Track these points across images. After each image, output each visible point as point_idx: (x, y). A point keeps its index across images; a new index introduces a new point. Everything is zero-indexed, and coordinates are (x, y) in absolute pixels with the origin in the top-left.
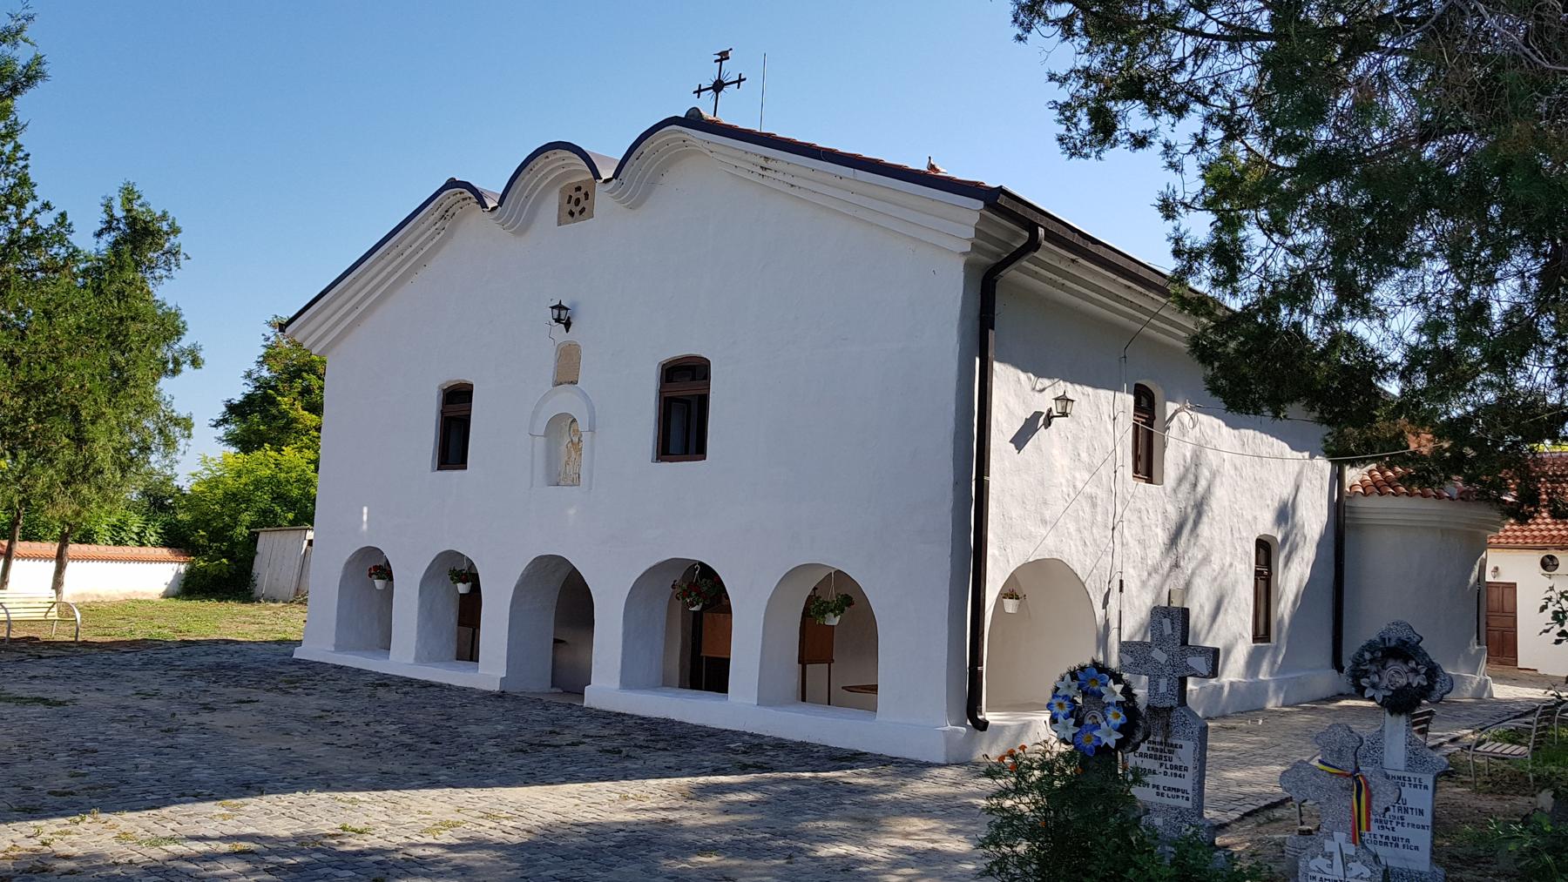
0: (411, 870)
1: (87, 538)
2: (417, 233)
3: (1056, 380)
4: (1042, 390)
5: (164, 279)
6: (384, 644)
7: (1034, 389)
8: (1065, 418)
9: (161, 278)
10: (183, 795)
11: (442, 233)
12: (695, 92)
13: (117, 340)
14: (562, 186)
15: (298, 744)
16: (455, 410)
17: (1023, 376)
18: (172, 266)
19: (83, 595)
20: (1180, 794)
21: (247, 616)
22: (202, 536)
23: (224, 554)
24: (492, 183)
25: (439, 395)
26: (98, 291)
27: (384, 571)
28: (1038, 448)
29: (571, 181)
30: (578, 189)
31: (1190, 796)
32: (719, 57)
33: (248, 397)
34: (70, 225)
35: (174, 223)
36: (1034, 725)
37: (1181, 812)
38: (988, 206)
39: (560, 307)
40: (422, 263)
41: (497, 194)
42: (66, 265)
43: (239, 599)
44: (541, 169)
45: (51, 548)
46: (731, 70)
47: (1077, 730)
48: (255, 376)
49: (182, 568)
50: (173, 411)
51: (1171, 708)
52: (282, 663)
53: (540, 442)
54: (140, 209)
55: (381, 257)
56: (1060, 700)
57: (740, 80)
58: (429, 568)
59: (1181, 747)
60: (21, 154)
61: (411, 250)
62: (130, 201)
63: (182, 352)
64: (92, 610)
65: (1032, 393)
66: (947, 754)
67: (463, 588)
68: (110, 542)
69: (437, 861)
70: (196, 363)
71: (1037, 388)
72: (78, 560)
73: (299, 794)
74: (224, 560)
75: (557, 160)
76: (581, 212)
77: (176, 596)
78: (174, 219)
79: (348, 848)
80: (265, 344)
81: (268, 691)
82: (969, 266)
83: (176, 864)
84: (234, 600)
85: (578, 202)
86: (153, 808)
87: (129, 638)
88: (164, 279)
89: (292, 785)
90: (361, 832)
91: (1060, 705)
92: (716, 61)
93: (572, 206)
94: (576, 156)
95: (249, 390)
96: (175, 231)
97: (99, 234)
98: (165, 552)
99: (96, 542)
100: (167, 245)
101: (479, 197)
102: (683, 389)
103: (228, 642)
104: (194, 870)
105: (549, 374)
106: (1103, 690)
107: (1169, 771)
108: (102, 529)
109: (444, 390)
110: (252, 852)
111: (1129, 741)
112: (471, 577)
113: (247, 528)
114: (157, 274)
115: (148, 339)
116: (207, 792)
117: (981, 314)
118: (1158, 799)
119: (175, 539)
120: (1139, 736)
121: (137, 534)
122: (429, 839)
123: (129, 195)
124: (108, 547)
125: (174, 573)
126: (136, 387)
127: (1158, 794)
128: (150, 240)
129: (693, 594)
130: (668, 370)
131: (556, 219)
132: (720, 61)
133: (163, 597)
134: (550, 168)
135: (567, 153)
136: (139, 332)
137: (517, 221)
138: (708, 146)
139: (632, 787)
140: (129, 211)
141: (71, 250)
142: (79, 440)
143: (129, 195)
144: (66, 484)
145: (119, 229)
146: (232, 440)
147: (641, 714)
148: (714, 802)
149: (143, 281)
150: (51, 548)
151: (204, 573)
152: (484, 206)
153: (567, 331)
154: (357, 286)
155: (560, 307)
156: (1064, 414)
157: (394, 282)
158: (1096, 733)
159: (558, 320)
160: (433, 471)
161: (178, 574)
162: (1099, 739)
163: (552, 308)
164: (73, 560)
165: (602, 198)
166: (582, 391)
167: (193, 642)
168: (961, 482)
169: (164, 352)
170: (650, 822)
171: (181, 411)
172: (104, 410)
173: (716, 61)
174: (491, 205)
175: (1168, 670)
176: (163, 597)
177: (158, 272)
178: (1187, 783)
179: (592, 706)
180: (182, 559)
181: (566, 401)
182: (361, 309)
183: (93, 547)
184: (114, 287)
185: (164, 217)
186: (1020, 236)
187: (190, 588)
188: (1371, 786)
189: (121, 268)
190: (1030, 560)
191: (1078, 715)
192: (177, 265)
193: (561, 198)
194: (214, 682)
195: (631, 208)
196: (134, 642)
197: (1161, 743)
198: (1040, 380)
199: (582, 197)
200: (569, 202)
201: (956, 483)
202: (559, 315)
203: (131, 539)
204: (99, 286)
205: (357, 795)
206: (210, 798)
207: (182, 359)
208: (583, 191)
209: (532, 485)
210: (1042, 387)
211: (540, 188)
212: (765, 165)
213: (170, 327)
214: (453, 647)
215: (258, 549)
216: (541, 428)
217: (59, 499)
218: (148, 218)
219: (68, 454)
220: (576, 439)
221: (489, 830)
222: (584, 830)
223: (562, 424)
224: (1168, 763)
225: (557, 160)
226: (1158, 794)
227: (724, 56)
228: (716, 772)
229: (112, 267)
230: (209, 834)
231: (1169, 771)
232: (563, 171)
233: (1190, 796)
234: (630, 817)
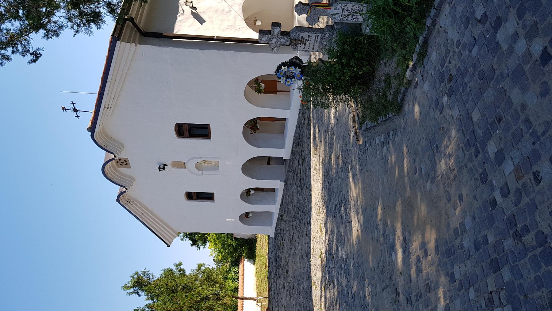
0: (331, 247)
1: (236, 290)
3: (179, 4)
4: (183, 11)
5: (153, 275)
6: (270, 214)
7: (183, 14)
8: (193, 2)
9: (153, 276)
10: (310, 295)
11: (135, 202)
12: (72, 102)
13: (174, 290)
14: (117, 167)
15: (298, 253)
16: (186, 131)
17: (179, 19)
18: (149, 273)
19: (254, 289)
20: (317, 37)
21: (261, 243)
22: (236, 254)
23: (241, 247)
24: (117, 189)
25: (190, 201)
26: (159, 296)
27: (247, 214)
28: (204, 12)
29: (115, 165)
30: (118, 162)
31: (317, 34)
32: (64, 110)
33: (189, 239)
34: (138, 308)
35: (134, 274)
36: (299, 19)
37: (322, 37)
38: (118, 39)
39: (159, 168)
40: (145, 207)
41: (120, 188)
42: (151, 308)
43: (256, 243)
44: (111, 174)
45: (239, 301)
47: (296, 78)
48: (183, 238)
49: (246, 260)
50: (196, 269)
51: (290, 39)
52: (275, 242)
53: (204, 172)
54: (130, 284)
55: (144, 220)
56: (287, 82)
57: (78, 117)
59: (302, 36)
61: (141, 211)
62: (128, 287)
63: (177, 269)
64: (259, 288)
65: (185, 15)
66: (307, 56)
67: (252, 192)
68: (238, 282)
69: (329, 238)
70: (180, 264)
71: (182, 12)
72: (243, 292)
73: (311, 263)
74: (243, 248)
75: (108, 170)
76: (126, 161)
77: (255, 261)
78: (133, 274)
79: (325, 260)
81: (283, 251)
82: (140, 43)
83: (326, 308)
84: (256, 244)
86: (313, 304)
87: (267, 282)
88: (153, 275)
89: (309, 261)
90: (321, 253)
91: (288, 82)
92: (66, 111)
93: (124, 164)
94: (106, 166)
95: (187, 239)
96: (137, 273)
97: (139, 295)
98: (241, 265)
99: (238, 286)
100: (142, 275)
101: (121, 193)
102: (186, 131)
103: (268, 254)
104: (328, 304)
105: (182, 170)
106: (284, 71)
107: (310, 40)
108: (233, 285)
109: (188, 199)
110: (325, 286)
111: (299, 64)
112: (249, 191)
113: (233, 241)
114: (152, 277)
115: (173, 280)
116: (309, 288)
118: (318, 43)
119: (236, 262)
120: (298, 61)
121: (235, 274)
122: (324, 235)
123: (126, 287)
124: (239, 283)
125: (247, 262)
126: (189, 283)
127: (316, 43)
128: (140, 281)
129: (254, 128)
130: (180, 136)
132: (66, 110)
133: (255, 265)
134: (111, 172)
135: (106, 168)
136: (171, 283)
137: (130, 181)
138: (101, 125)
139: (313, 165)
140: (131, 287)
141: (146, 307)
142: (206, 298)
143: (126, 287)
144: (220, 300)
145: (137, 290)
146: (204, 243)
147: (292, 143)
148: (318, 142)
149: (154, 281)
150: (239, 301)
151: (247, 254)
152: (125, 192)
155: (159, 168)
156: (192, 2)
157: (153, 215)
158: (297, 74)
159: (164, 169)
160: (214, 202)
162: (298, 73)
163: (160, 170)
164: (243, 295)
165: (122, 155)
166: (188, 161)
167: (268, 264)
168: (217, 48)
169: (178, 274)
170: (322, 167)
171: (196, 267)
172: (197, 292)
173: (66, 111)
174: (124, 189)
175: (279, 39)
176: (255, 265)
177: (151, 277)
178: (313, 35)
179: (289, 157)
180: (243, 260)
181: (191, 166)
182: (162, 224)
183: (239, 287)
184: (157, 291)
185: (132, 277)
186: (128, 24)
187: (252, 257)
188: (314, 2)
189: (150, 289)
190: (243, 17)
191: (291, 77)
193: (121, 167)
194: (280, 265)
195: (123, 147)
196: (268, 281)
197: (301, 42)
198: (179, 11)
200: (123, 165)
201: (217, 49)
202: (162, 168)
203: (237, 276)
204: (157, 296)
205: (312, 247)
206: (311, 287)
207: (180, 269)
208: (118, 161)
209: (219, 174)
210: (182, 10)
211: (115, 172)
212: (107, 108)
213: (169, 273)
214: (270, 193)
215: (240, 237)
216: (200, 172)
217: (224, 302)
218: (133, 281)
219: (211, 302)
220: (204, 162)
221: (323, 216)
222: (323, 190)
223: (198, 166)
224: (307, 40)
225: (108, 170)
226: (316, 43)
227: (64, 108)
228: (310, 134)
229: (150, 292)
230: (320, 294)
231: (310, 40)
232: (111, 168)
233: (317, 34)
234: (321, 172)
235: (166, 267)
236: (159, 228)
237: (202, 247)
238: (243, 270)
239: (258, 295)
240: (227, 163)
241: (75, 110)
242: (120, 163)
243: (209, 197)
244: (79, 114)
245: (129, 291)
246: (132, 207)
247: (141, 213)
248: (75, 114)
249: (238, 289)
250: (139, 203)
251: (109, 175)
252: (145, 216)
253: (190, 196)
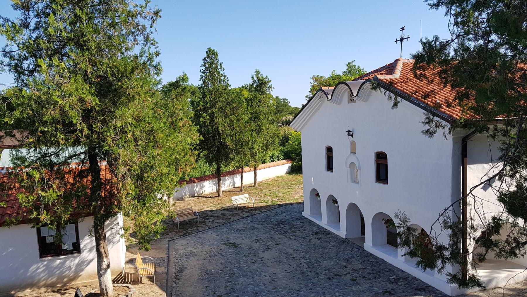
2: (315, 102)
27: (318, 195)
39: (349, 131)
40: (318, 109)
46: (405, 34)
49: (290, 165)
53: (349, 169)
57: (408, 38)
58: (328, 198)
60: (226, 78)
61: (314, 106)
80: (311, 85)
92: (401, 30)
96: (269, 81)
98: (285, 161)
117: (462, 152)
121: (277, 157)
123: (257, 73)
131: (347, 102)
133: (286, 174)
143: (257, 73)
151: (295, 166)
152: (328, 98)
154: (303, 115)
155: (349, 131)
159: (349, 135)
161: (289, 166)
163: (347, 131)
173: (401, 30)
176: (286, 174)
181: (353, 159)
183: (266, 164)
192: (272, 90)
193: (348, 95)
209: (348, 182)
211: (342, 93)
223: (352, 165)
227: (403, 29)
235: (277, 96)
236: (307, 113)
237: (312, 81)
238: (280, 164)
239: (259, 183)
240: (357, 192)
241: (402, 40)
243: (330, 167)
244: (399, 42)
245: (255, 76)
246: (316, 100)
247: (313, 106)
248: (399, 39)
249: (264, 163)
250: (321, 104)
252: (310, 109)
253: (329, 150)
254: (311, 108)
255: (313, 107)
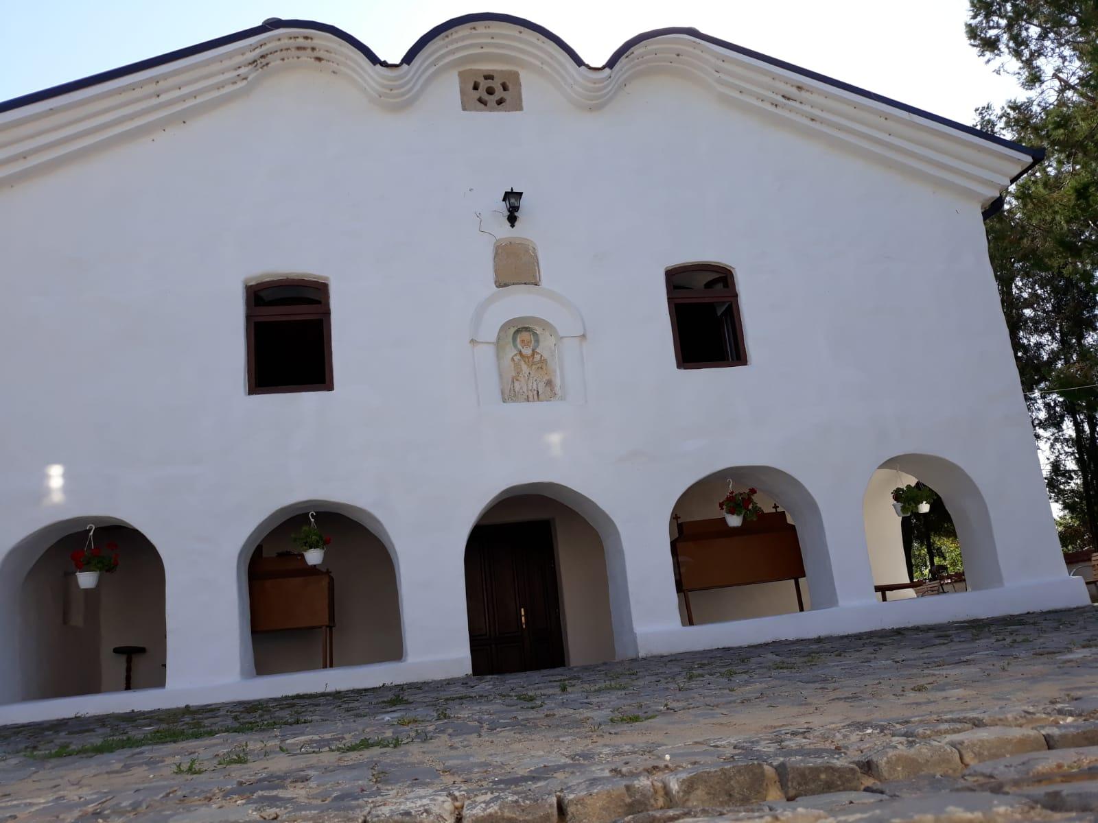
44: (463, 39)
61: (176, 93)
76: (505, 88)
85: (490, 91)
153: (513, 226)
199: (489, 83)
220: (527, 351)
242: (482, 92)
246: (227, 63)
251: (513, 30)
254: (149, 97)
255: (163, 98)
